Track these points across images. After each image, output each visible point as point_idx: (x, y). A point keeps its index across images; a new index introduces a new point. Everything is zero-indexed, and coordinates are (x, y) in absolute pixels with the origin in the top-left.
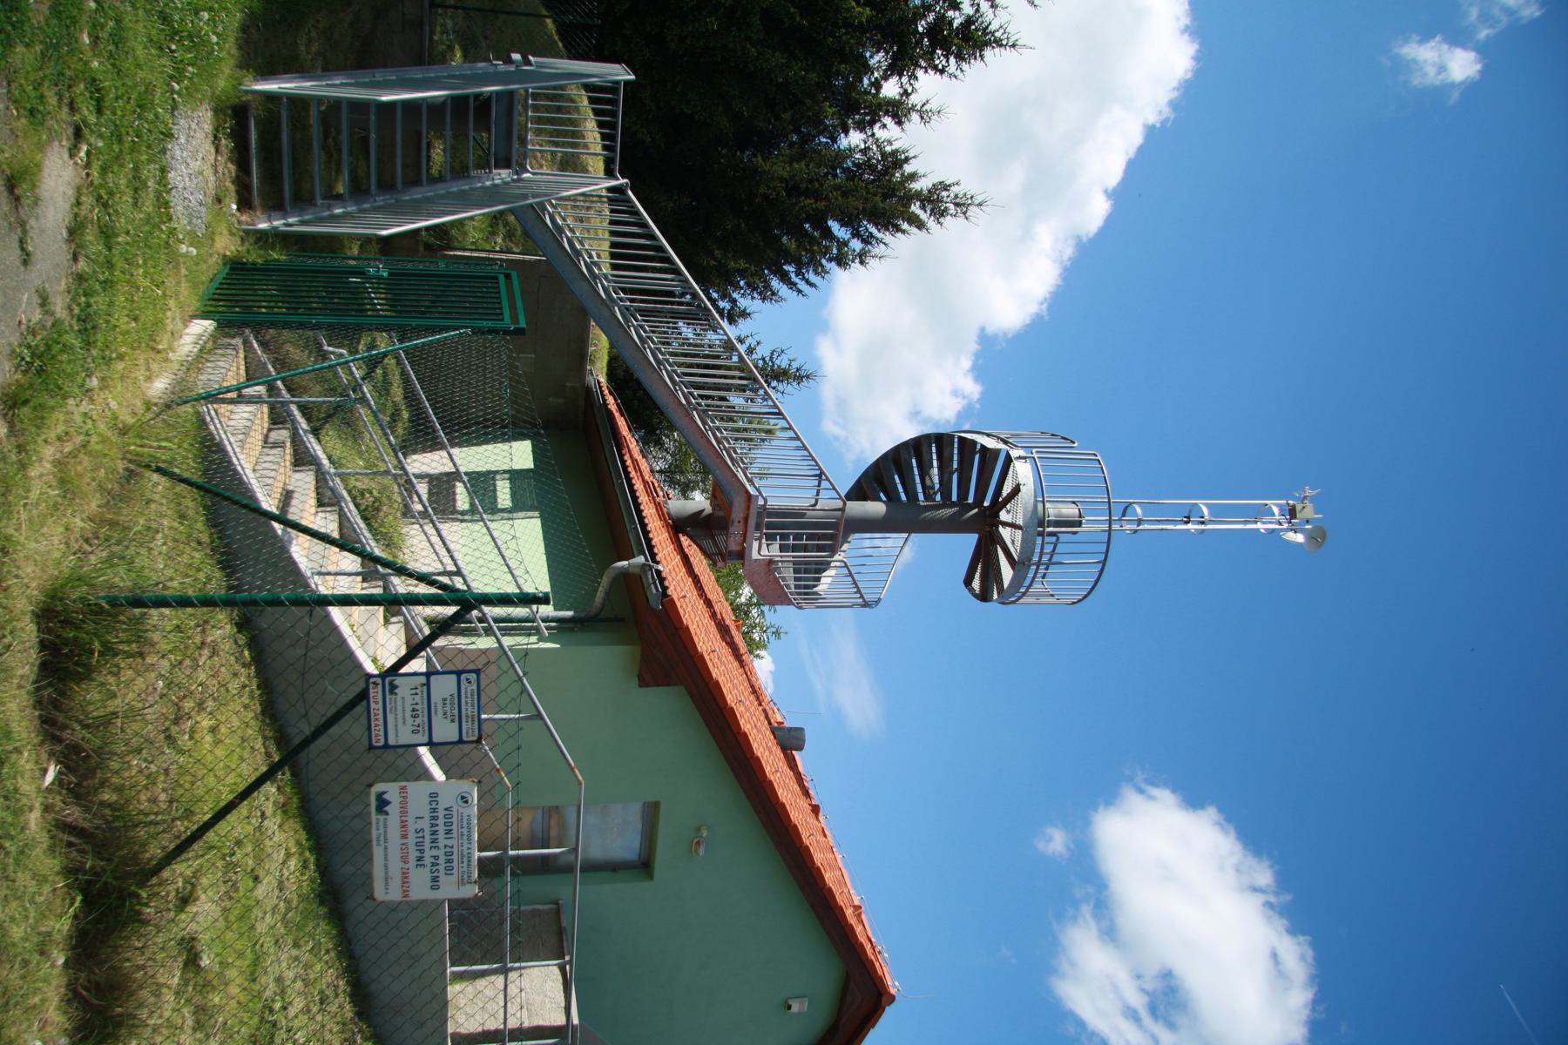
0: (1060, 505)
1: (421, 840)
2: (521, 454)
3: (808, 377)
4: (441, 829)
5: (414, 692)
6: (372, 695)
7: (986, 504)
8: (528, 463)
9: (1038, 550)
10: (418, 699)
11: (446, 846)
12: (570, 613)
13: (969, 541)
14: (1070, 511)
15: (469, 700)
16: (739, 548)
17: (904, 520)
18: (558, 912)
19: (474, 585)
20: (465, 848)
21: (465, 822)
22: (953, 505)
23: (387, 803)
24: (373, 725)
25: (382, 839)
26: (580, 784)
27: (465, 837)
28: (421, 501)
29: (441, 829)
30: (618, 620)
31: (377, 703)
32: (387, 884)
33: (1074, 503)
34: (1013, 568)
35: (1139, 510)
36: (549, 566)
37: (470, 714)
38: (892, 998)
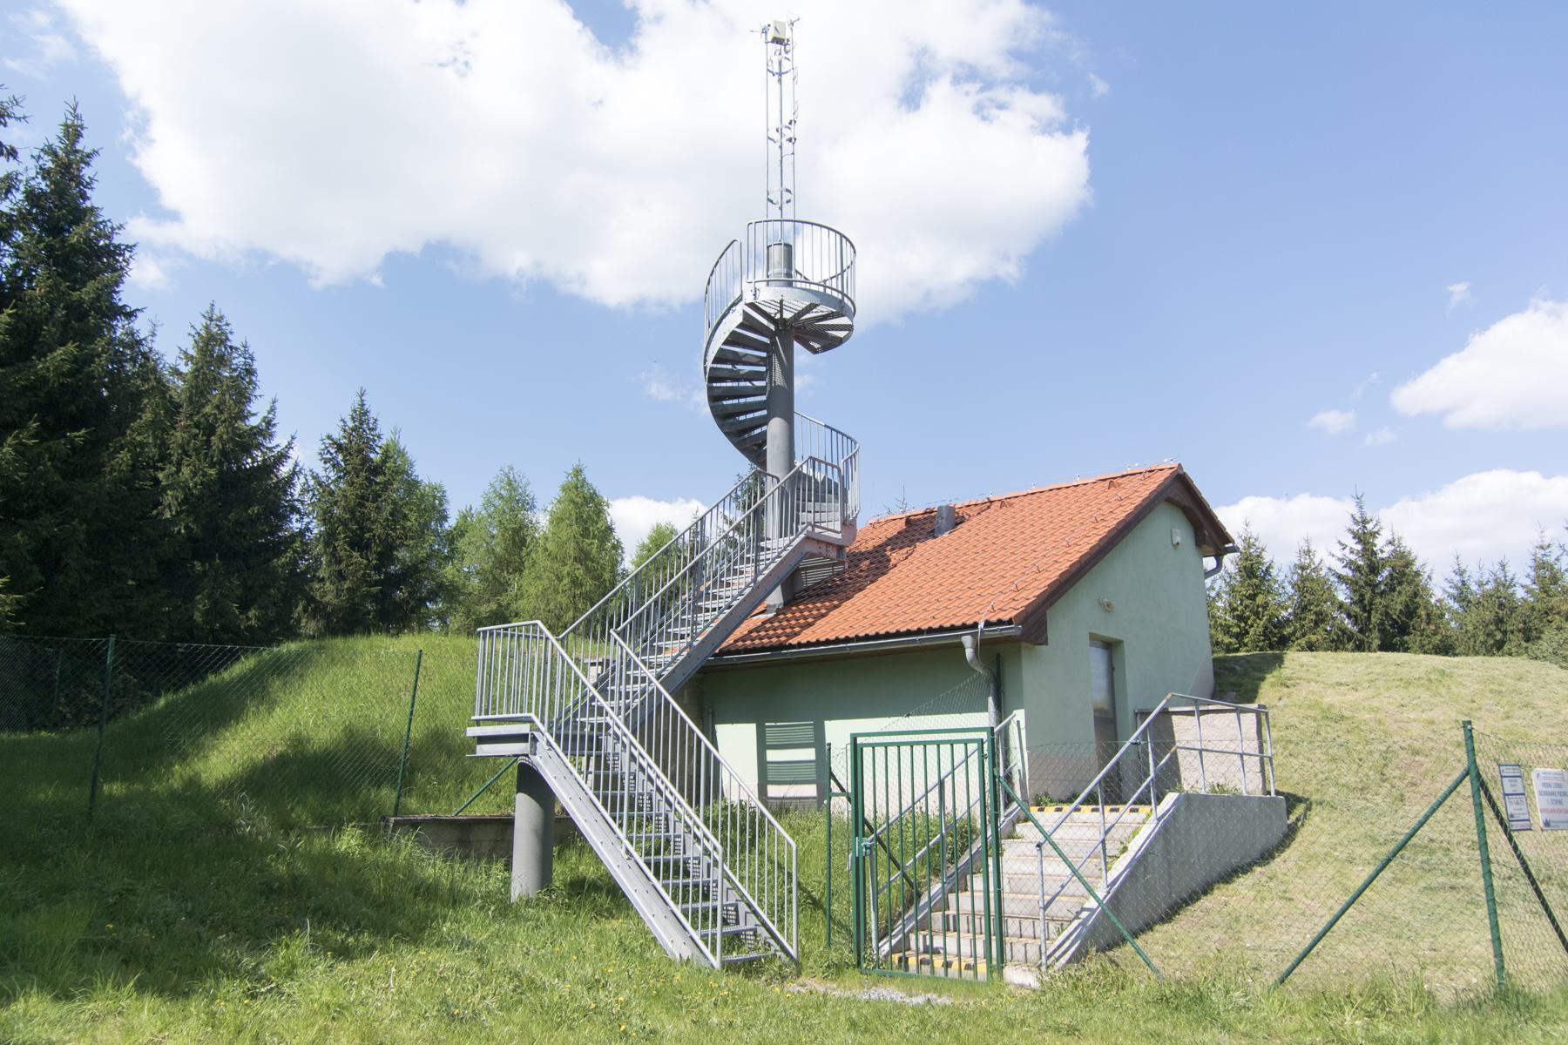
7: (772, 327)
12: (991, 700)
17: (782, 403)
22: (769, 357)
34: (843, 316)
36: (946, 713)
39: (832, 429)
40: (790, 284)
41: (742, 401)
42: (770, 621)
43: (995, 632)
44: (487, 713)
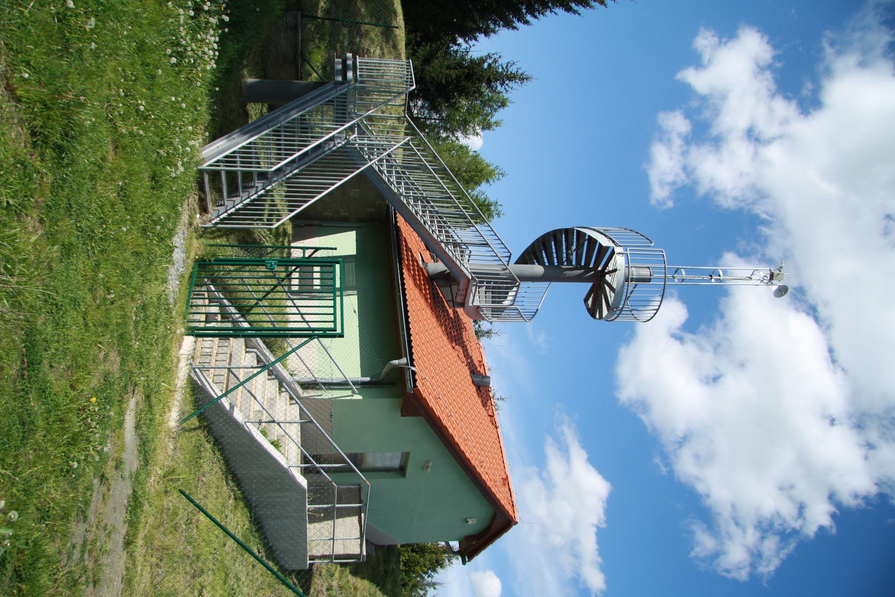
0: (640, 269)
3: (527, 79)
7: (600, 269)
9: (622, 303)
12: (368, 379)
13: (588, 286)
14: (645, 273)
17: (553, 275)
18: (360, 489)
19: (316, 376)
22: (581, 268)
33: (648, 268)
35: (684, 273)
39: (536, 313)
40: (627, 280)
41: (555, 255)
42: (418, 265)
43: (409, 376)
44: (360, 69)
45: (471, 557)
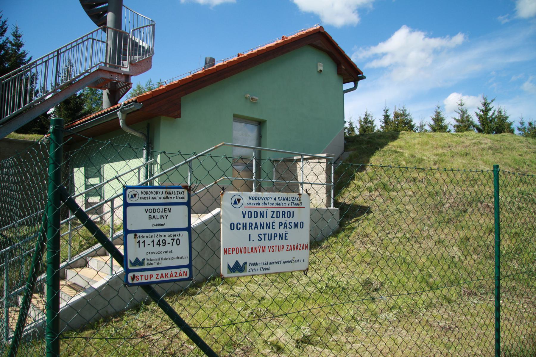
1: (267, 236)
2: (79, 174)
4: (259, 220)
5: (142, 245)
6: (144, 281)
8: (82, 169)
10: (148, 241)
11: (272, 217)
12: (145, 152)
15: (151, 196)
16: (124, 77)
20: (275, 202)
21: (254, 202)
23: (237, 263)
24: (172, 278)
25: (264, 266)
26: (224, 144)
27: (266, 202)
28: (97, 218)
29: (259, 220)
30: (149, 126)
31: (151, 276)
32: (297, 261)
37: (164, 196)
38: (321, 27)
45: (358, 72)
